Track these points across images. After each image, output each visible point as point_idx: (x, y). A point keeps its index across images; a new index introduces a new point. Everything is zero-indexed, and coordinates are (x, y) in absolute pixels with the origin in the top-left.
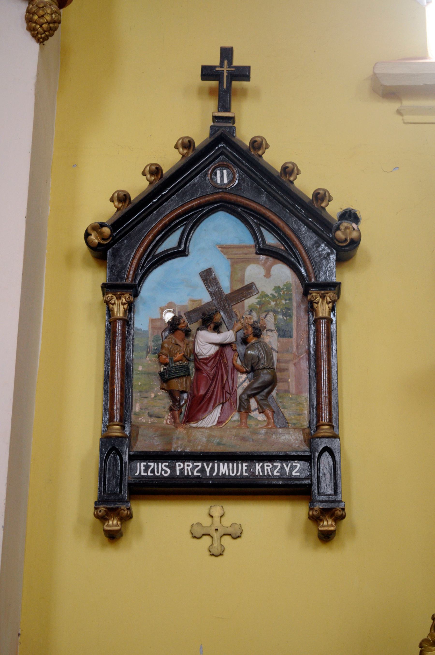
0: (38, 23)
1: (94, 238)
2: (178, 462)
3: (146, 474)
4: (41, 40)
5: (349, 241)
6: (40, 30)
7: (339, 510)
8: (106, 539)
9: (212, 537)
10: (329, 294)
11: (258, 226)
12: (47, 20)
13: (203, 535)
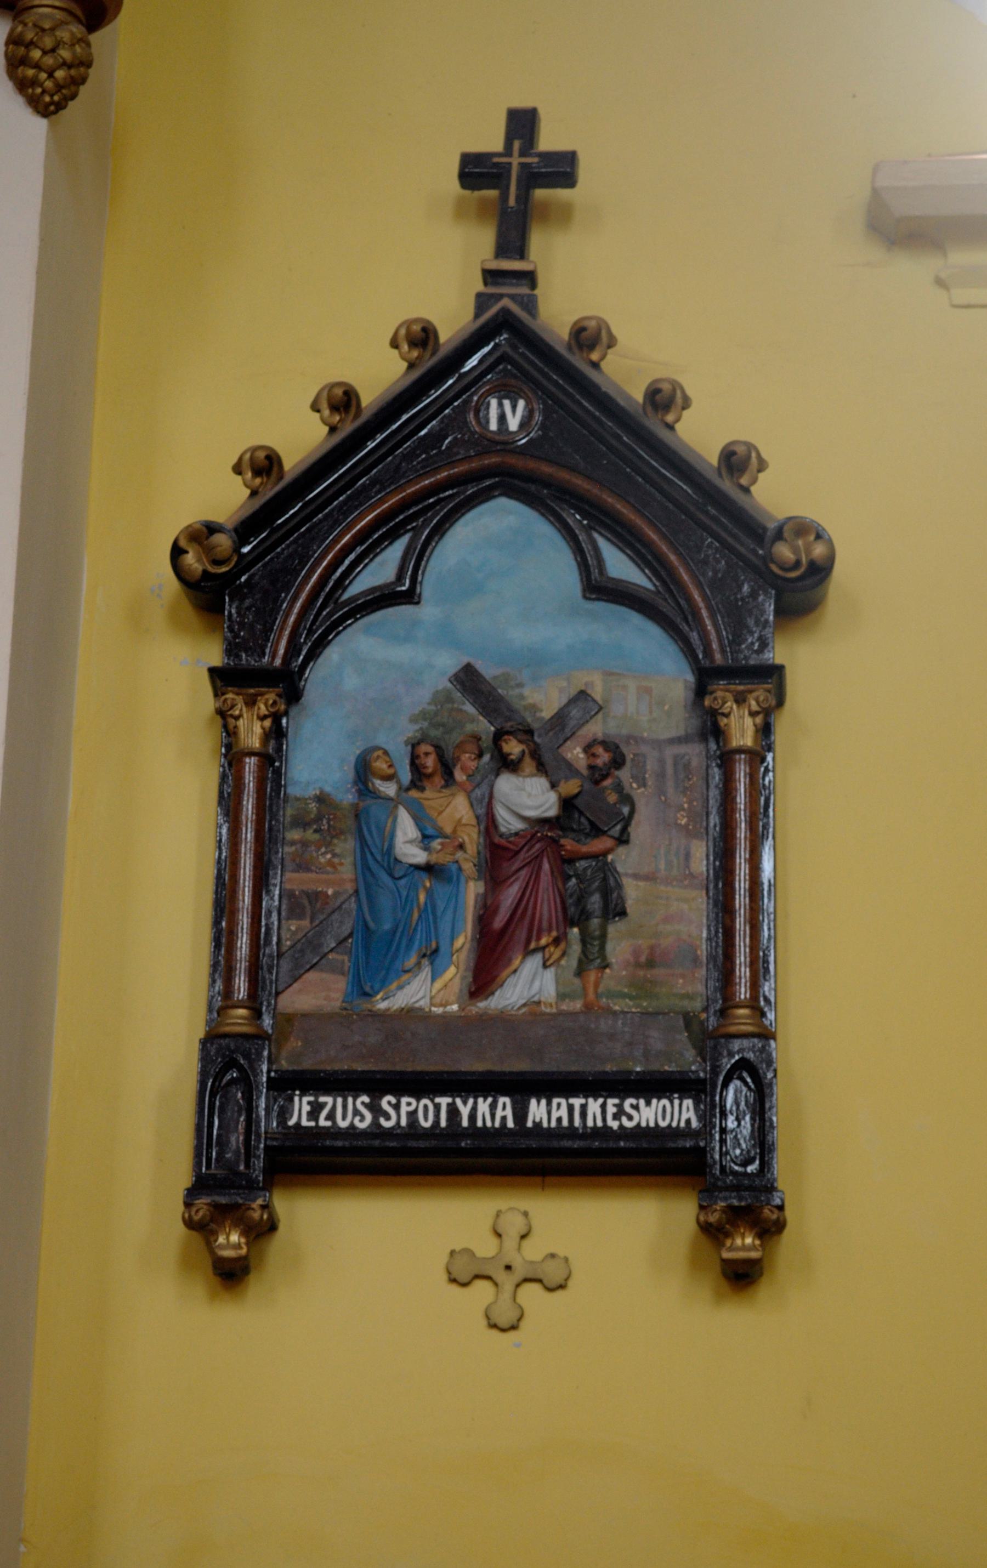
0: (43, 67)
1: (191, 559)
3: (312, 1124)
4: (52, 108)
5: (802, 570)
6: (49, 84)
8: (216, 1280)
9: (496, 1284)
10: (755, 694)
11: (589, 528)
13: (477, 1277)
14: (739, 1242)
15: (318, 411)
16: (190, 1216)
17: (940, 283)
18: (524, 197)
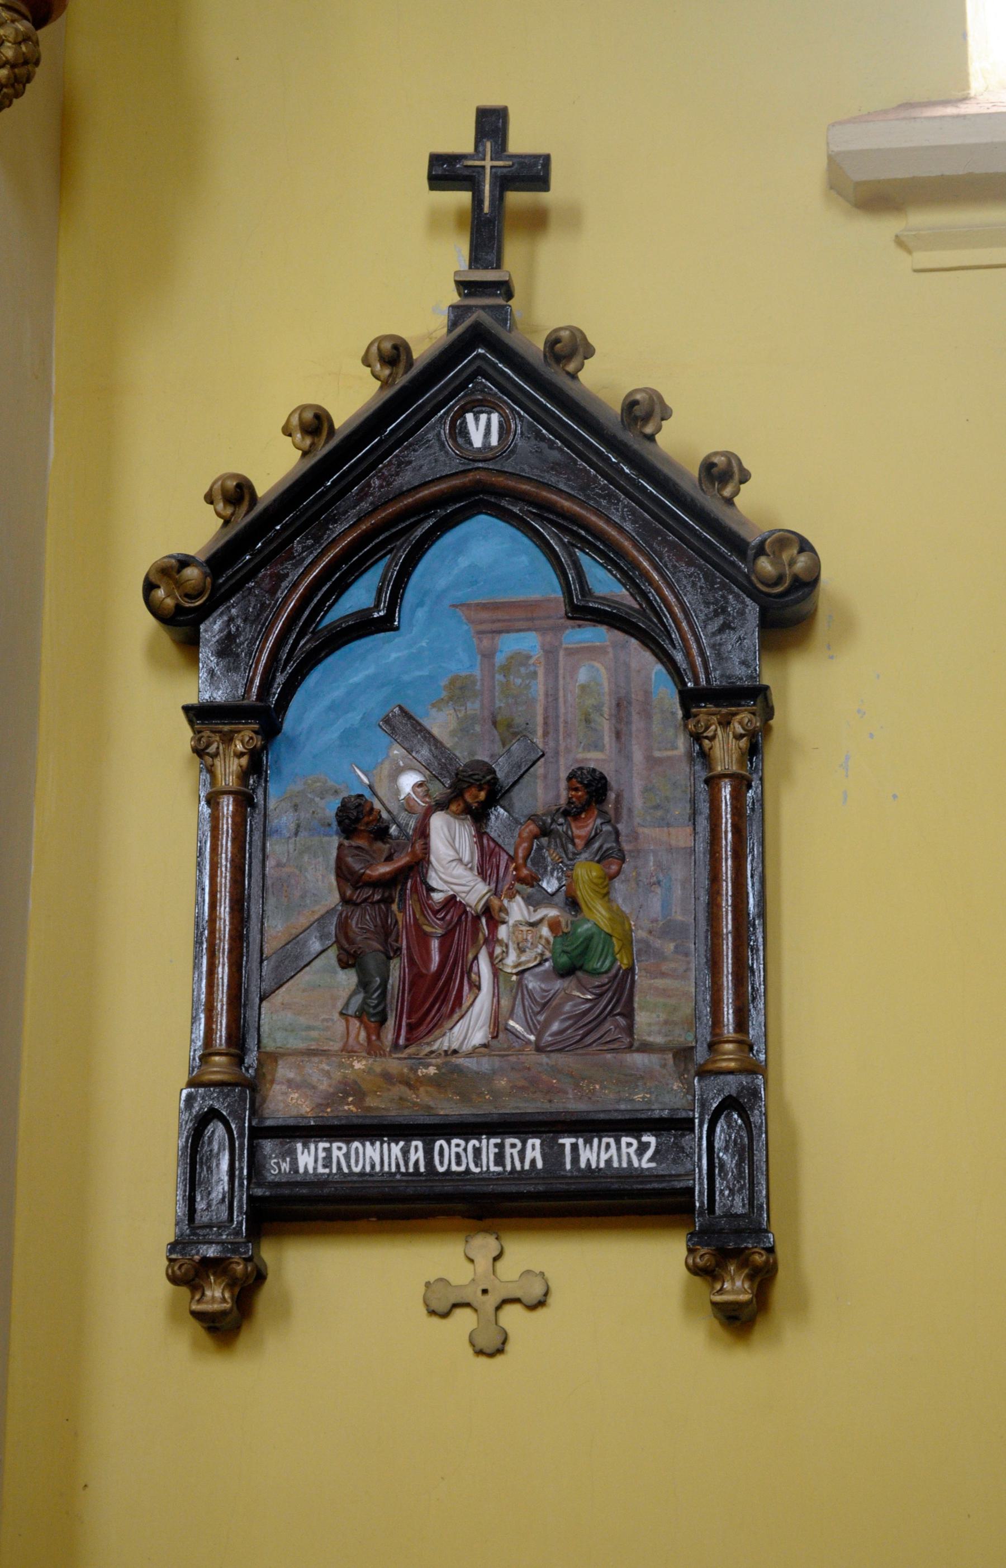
2: (627, 1136)
7: (760, 1253)
10: (738, 717)
12: (6, 58)
13: (498, 1308)
14: (727, 1285)
15: (212, 503)
16: (173, 1272)
17: (900, 242)
18: (498, 200)
